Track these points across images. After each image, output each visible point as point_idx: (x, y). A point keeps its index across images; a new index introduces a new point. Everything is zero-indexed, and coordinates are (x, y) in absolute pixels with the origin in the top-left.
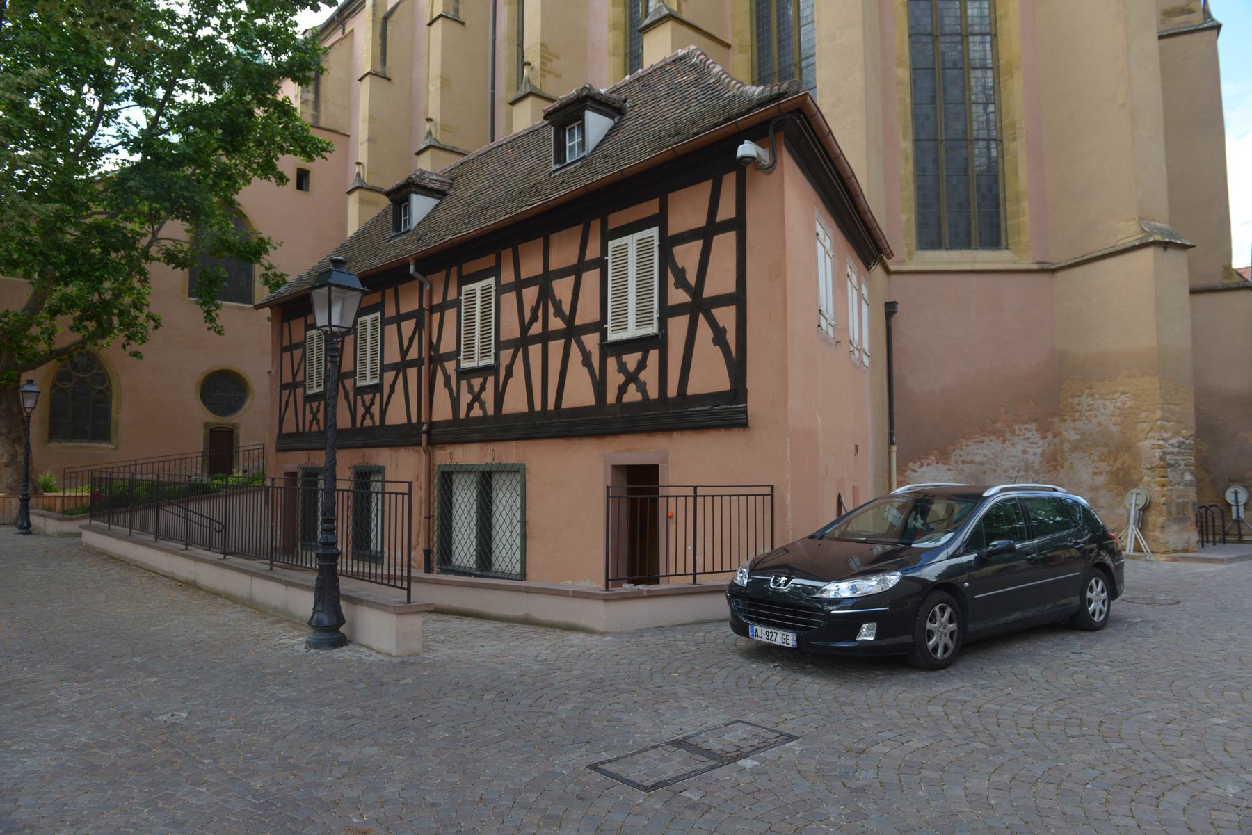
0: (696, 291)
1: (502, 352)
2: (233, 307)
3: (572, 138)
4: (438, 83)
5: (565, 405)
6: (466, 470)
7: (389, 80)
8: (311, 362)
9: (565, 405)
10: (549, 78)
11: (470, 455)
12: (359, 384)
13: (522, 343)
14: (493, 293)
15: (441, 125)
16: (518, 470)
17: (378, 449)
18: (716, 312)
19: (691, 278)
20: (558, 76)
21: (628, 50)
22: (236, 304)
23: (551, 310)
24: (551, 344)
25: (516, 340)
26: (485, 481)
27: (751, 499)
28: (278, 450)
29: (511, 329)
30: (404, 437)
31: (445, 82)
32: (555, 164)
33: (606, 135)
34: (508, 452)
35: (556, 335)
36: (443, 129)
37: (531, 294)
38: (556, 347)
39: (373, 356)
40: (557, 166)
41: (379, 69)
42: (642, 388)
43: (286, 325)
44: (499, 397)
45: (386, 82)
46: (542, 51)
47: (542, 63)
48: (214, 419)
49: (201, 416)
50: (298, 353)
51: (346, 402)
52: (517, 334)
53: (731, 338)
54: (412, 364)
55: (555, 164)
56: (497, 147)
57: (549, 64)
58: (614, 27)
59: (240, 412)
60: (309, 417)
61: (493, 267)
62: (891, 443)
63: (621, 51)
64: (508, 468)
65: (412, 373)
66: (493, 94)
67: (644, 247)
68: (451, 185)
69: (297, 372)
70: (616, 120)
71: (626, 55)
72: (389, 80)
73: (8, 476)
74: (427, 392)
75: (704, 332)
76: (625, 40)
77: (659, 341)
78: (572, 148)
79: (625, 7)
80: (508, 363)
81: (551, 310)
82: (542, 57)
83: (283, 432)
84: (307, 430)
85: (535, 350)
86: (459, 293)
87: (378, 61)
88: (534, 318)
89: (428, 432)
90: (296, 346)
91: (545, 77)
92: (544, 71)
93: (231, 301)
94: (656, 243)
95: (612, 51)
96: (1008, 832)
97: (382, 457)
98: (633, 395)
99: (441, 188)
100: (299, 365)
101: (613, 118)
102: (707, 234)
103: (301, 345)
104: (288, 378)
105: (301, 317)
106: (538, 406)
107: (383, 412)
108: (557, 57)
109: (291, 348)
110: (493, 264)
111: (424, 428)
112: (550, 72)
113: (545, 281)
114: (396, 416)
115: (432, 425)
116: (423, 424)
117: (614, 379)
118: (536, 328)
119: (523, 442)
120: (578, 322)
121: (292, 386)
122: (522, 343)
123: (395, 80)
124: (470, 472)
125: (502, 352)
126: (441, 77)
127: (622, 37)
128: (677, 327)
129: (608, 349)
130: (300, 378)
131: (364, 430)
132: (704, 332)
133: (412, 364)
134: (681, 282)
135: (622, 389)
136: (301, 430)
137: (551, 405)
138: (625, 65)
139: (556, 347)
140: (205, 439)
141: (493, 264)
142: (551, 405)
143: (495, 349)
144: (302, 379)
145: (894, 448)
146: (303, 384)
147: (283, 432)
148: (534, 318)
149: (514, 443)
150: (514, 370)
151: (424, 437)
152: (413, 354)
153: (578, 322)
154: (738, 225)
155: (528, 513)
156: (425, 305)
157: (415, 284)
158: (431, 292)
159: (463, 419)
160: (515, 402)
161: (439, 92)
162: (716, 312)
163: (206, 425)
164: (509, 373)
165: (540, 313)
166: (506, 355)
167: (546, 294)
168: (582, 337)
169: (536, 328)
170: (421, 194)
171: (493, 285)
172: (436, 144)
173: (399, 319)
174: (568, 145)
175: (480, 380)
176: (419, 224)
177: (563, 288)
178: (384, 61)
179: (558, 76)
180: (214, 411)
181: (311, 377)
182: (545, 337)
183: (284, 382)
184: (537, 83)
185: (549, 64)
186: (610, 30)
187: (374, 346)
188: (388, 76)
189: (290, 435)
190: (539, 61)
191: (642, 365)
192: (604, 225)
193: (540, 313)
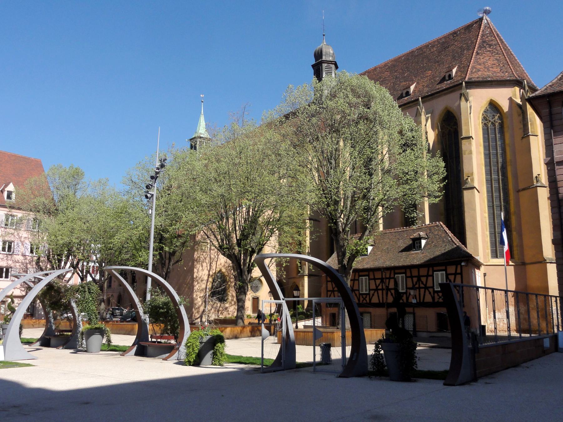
3: (417, 244)
18: (429, 289)
19: (424, 283)
23: (421, 283)
35: (422, 288)
37: (415, 280)
42: (366, 300)
44: (370, 300)
53: (371, 297)
62: (487, 307)
67: (442, 275)
73: (560, 184)
75: (427, 292)
77: (369, 294)
81: (421, 283)
88: (416, 284)
94: (405, 276)
96: (3, 309)
98: (365, 301)
102: (455, 274)
106: (381, 302)
110: (404, 271)
113: (419, 277)
114: (375, 300)
117: (361, 299)
118: (417, 286)
129: (360, 294)
132: (427, 292)
133: (380, 289)
134: (422, 283)
135: (363, 301)
137: (422, 301)
141: (404, 271)
145: (487, 308)
154: (461, 274)
162: (429, 289)
165: (418, 283)
167: (419, 280)
181: (362, 287)
182: (419, 288)
191: (366, 297)
192: (359, 274)
193: (418, 283)
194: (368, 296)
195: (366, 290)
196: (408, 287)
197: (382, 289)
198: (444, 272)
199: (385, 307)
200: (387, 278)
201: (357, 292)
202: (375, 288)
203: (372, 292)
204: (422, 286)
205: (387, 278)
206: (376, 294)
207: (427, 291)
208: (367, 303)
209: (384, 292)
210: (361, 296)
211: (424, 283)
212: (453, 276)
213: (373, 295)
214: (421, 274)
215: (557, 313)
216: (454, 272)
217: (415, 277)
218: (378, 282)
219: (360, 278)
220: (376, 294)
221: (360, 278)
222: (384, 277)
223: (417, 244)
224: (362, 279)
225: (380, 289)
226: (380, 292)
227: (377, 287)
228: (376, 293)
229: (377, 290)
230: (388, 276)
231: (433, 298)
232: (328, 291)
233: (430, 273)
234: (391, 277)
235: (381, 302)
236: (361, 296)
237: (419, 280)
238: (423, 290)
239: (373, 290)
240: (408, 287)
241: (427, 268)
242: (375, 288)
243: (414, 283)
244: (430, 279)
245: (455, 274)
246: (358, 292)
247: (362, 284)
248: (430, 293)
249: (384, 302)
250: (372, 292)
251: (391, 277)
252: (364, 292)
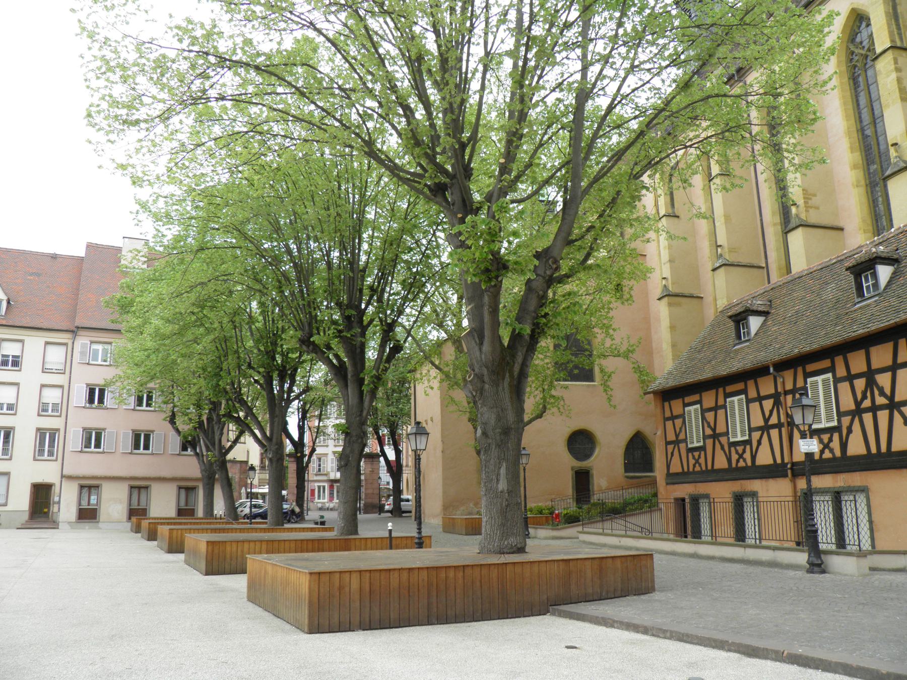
0: (891, 398)
1: (842, 418)
2: (583, 385)
3: (867, 281)
4: (723, 219)
5: (894, 448)
6: (823, 491)
7: (678, 217)
8: (691, 427)
9: (894, 448)
10: (811, 211)
11: (821, 481)
12: (732, 440)
13: (858, 412)
14: (832, 383)
15: (729, 248)
16: (864, 490)
17: (752, 481)
19: (888, 391)
20: (817, 208)
21: (868, 181)
22: (584, 383)
23: (876, 392)
24: (879, 413)
25: (852, 411)
26: (837, 496)
27: (180, 531)
28: (667, 484)
29: (848, 403)
30: (774, 471)
31: (727, 218)
32: (858, 297)
33: (891, 278)
34: (856, 479)
35: (882, 407)
36: (730, 251)
37: (860, 384)
38: (883, 416)
39: (742, 422)
40: (860, 299)
41: (670, 211)
42: (832, 451)
43: (666, 404)
44: (844, 446)
45: (676, 219)
46: (804, 194)
47: (805, 202)
48: (578, 464)
49: (568, 462)
50: (678, 422)
51: (722, 452)
52: (853, 407)
54: (774, 426)
55: (858, 297)
56: (798, 278)
57: (810, 201)
58: (855, 167)
59: (592, 458)
60: (692, 462)
61: (829, 368)
63: (863, 183)
64: (857, 489)
65: (774, 433)
66: (761, 220)
68: (770, 306)
69: (679, 433)
70: (895, 266)
71: (867, 185)
72: (678, 217)
74: (788, 444)
76: (865, 175)
77: (837, 429)
78: (868, 287)
79: (861, 152)
80: (848, 425)
81: (876, 392)
82: (804, 198)
83: (671, 472)
84: (691, 470)
85: (868, 418)
86: (806, 383)
87: (669, 206)
88: (864, 397)
89: (791, 469)
90: (677, 417)
91: (808, 211)
92: (808, 207)
93: (581, 381)
95: (855, 183)
97: (756, 485)
99: (766, 310)
100: (681, 429)
101: (893, 265)
102: (715, 409)
103: (682, 416)
104: (671, 437)
105: (679, 398)
106: (874, 450)
107: (753, 458)
108: (815, 195)
109: (673, 418)
110: (829, 365)
111: (789, 466)
112: (811, 207)
113: (870, 375)
114: (764, 458)
115: (793, 464)
116: (787, 464)
117: (735, 457)
118: (867, 403)
119: (865, 472)
120: (897, 399)
121: (677, 442)
122: (858, 412)
123: (682, 216)
124: (827, 492)
125: (842, 418)
126: (724, 216)
127: (862, 173)
128: (709, 442)
130: (682, 436)
131: (738, 469)
133: (774, 426)
134: (882, 393)
135: (738, 461)
136: (686, 469)
137: (884, 448)
138: (867, 192)
139: (883, 416)
140: (572, 478)
141: (829, 365)
142: (884, 448)
143: (837, 416)
144: (684, 437)
146: (685, 441)
147: (671, 472)
148: (864, 397)
149: (858, 473)
150: (853, 428)
151: (789, 472)
152: (774, 420)
153: (897, 399)
155: (873, 516)
156: (779, 390)
157: (771, 378)
158: (784, 383)
159: (817, 460)
160: (856, 447)
161: (724, 227)
163: (572, 469)
164: (850, 431)
165: (868, 394)
166: (846, 421)
167: (871, 383)
168: (902, 408)
169: (867, 403)
170: (755, 315)
171: (831, 377)
172: (727, 262)
173: (760, 399)
174: (864, 285)
175: (828, 435)
176: (756, 334)
177: (884, 380)
178: (673, 205)
179: (817, 208)
180: (577, 458)
182: (874, 409)
183: (668, 440)
184: (803, 216)
185: (810, 201)
186: (851, 170)
187: (741, 416)
188: (677, 214)
189: (677, 474)
190: (803, 201)
191: (831, 440)
192: (724, 390)
193: (868, 394)
194: (836, 436)
195: (829, 419)
196: (842, 410)
197: (779, 426)
198: (743, 396)
199: (786, 476)
200: (786, 393)
201: (723, 440)
202: (762, 423)
203: (756, 435)
204: (880, 400)
205: (786, 393)
206: (856, 426)
207: (896, 413)
208: (834, 459)
209: (784, 431)
210: (733, 449)
211: (888, 391)
212: (712, 413)
213: (759, 442)
214: (875, 365)
215: (191, 523)
216: (713, 404)
217: (859, 376)
218: (768, 404)
219: (809, 380)
220: (856, 426)
221: (809, 380)
222: (780, 389)
223: (867, 281)
224: (733, 401)
225: (867, 410)
226: (774, 433)
227: (858, 404)
228: (857, 420)
229: (766, 428)
230: (789, 386)
231: (729, 460)
232: (668, 443)
233: (721, 402)
234: (798, 386)
235: (874, 450)
236: (733, 449)
237: (871, 383)
238: (887, 412)
239: (847, 413)
240: (842, 410)
241: (829, 360)
242: (762, 423)
243: (859, 396)
244: (721, 412)
245: (715, 409)
246: (726, 438)
247: (733, 415)
248: (722, 448)
249: (786, 461)
250: (846, 421)
251: (798, 386)
252: (739, 438)
